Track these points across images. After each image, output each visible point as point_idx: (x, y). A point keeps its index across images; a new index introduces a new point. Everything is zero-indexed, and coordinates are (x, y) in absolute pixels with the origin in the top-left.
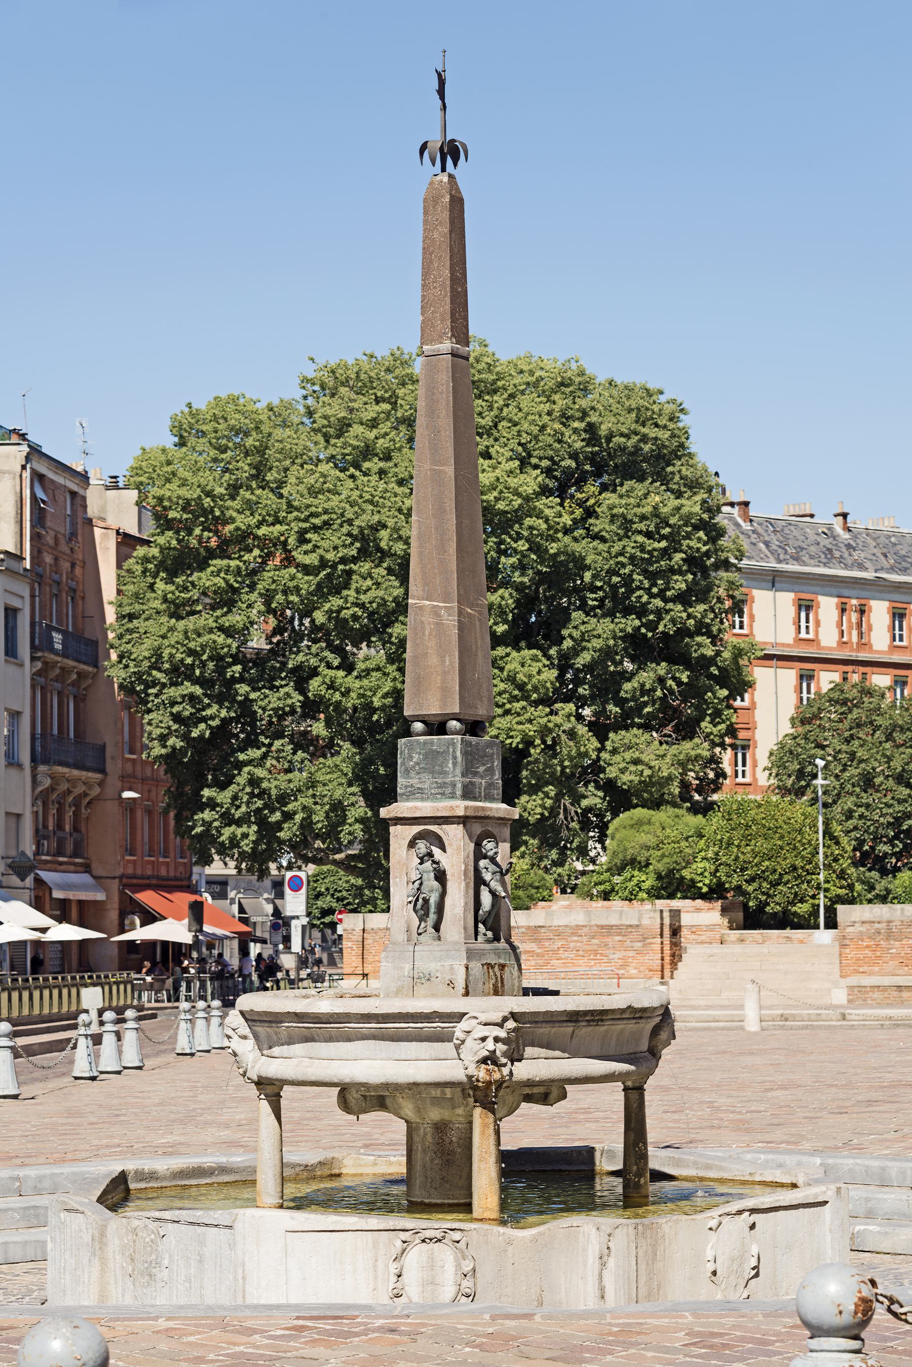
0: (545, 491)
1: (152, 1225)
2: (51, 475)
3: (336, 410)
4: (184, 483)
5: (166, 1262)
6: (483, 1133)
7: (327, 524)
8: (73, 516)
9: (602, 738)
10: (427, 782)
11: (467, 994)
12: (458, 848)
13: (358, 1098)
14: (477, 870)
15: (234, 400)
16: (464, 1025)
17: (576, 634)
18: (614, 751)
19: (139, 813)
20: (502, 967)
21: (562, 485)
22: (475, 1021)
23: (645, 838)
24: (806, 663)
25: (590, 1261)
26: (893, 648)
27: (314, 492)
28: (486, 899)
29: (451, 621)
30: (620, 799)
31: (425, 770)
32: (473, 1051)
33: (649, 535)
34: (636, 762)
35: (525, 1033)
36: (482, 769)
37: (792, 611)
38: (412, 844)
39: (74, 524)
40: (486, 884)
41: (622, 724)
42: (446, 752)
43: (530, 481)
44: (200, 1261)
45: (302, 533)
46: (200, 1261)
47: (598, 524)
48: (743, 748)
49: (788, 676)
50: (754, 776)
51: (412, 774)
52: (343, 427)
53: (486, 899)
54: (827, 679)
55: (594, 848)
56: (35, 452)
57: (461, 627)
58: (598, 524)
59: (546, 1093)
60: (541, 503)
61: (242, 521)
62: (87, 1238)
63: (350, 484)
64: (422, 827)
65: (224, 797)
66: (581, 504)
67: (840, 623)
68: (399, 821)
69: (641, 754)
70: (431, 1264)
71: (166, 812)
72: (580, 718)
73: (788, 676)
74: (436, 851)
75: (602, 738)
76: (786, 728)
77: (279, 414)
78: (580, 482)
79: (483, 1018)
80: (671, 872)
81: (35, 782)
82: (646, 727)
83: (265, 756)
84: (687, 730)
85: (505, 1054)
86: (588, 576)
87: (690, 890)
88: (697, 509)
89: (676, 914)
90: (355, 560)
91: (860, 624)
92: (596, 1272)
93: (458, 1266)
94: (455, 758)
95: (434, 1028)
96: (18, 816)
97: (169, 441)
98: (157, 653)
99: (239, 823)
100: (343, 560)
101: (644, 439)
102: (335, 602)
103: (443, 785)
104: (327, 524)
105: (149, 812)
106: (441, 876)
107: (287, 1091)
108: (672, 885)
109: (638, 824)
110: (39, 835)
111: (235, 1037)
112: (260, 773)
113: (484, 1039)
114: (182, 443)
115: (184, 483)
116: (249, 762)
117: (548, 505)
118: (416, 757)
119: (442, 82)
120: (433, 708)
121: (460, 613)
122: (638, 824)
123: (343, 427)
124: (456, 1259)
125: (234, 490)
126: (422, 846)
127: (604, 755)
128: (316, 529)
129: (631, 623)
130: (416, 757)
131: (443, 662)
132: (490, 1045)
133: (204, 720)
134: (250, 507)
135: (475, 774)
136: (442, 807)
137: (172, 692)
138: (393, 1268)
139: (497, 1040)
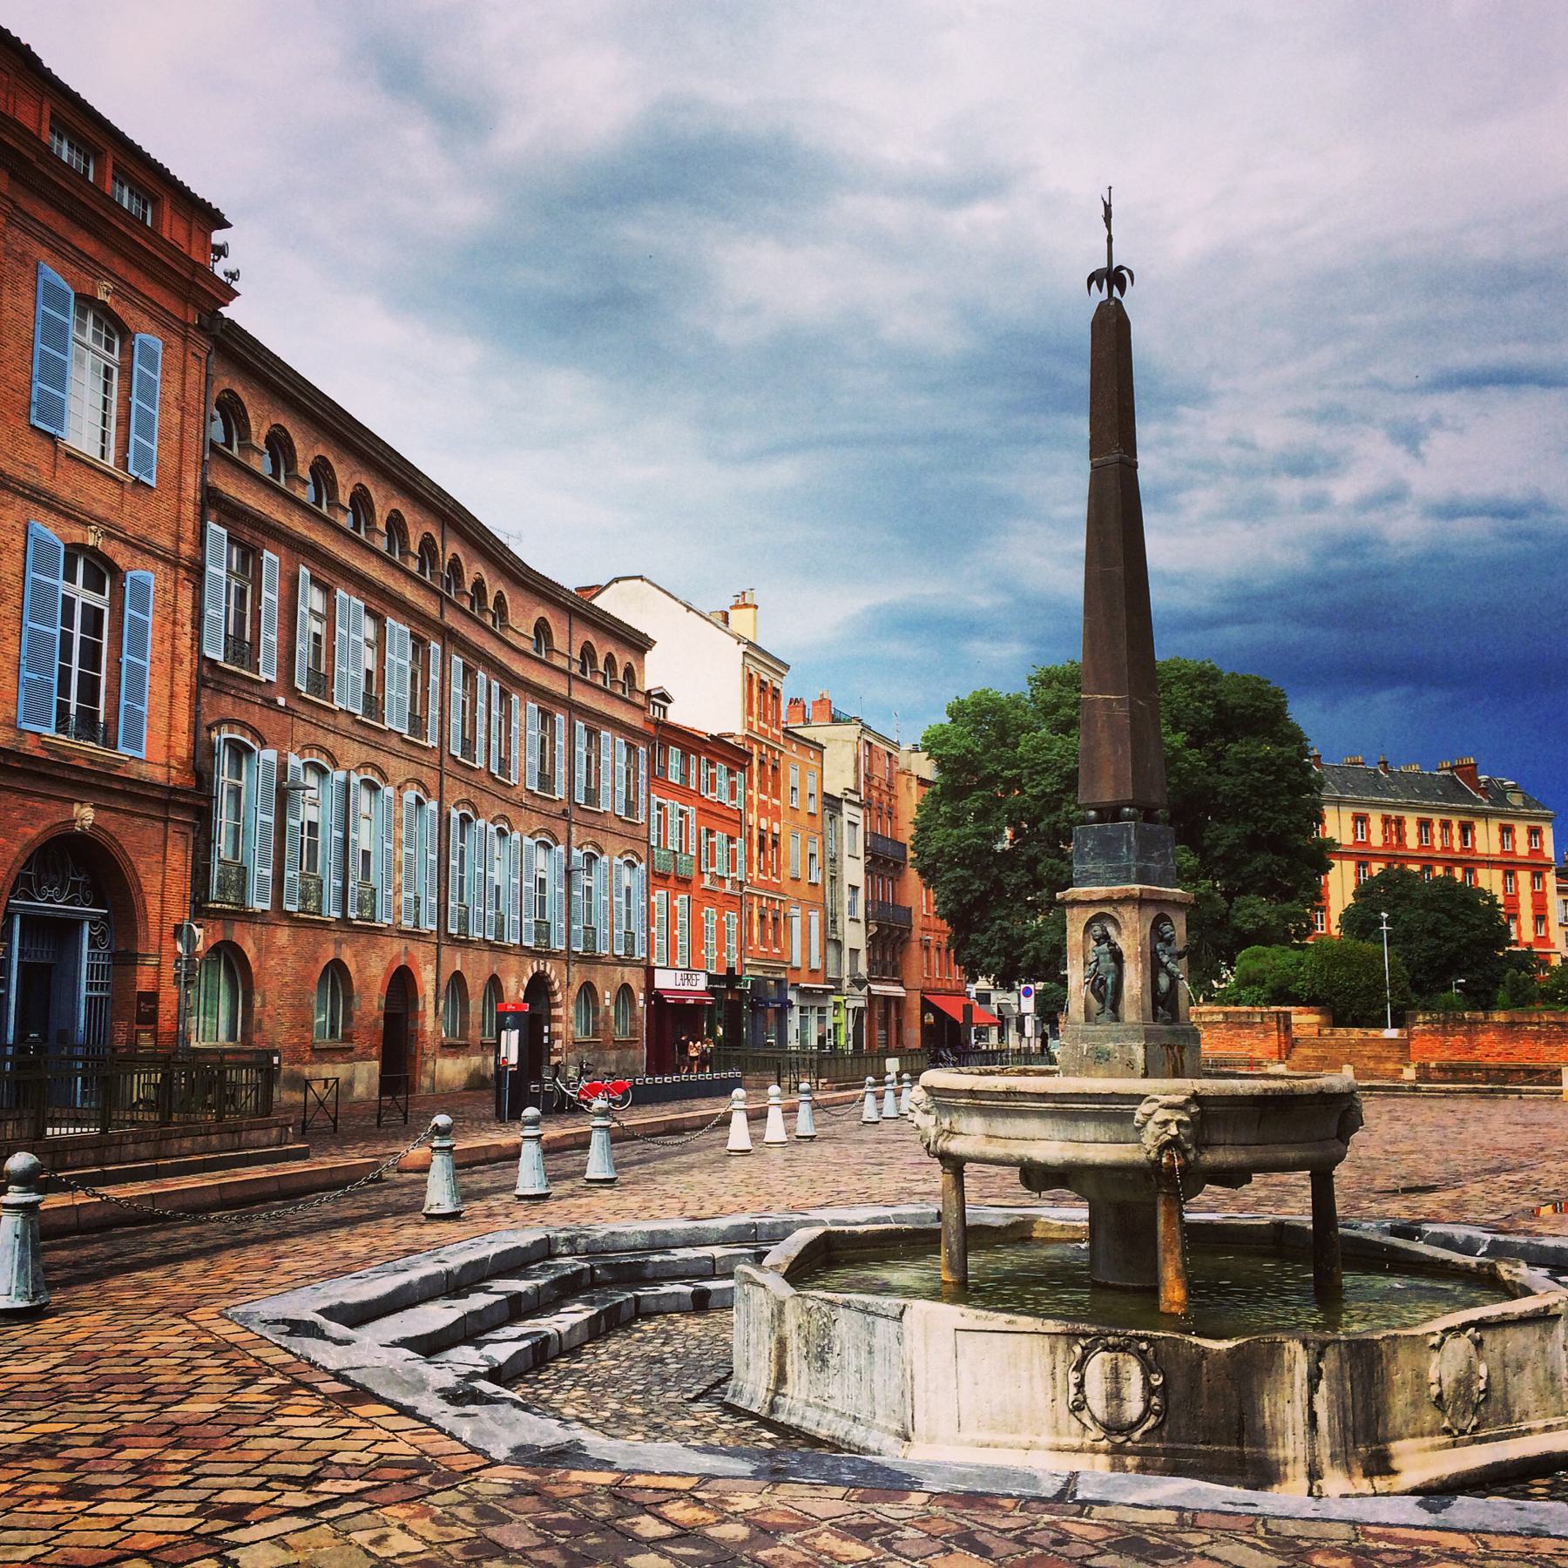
0: (1189, 745)
1: (825, 1308)
2: (875, 743)
3: (1048, 696)
4: (955, 746)
5: (837, 1349)
6: (1167, 1221)
7: (1046, 770)
8: (891, 768)
9: (1230, 901)
10: (1099, 866)
11: (1145, 1076)
12: (1134, 931)
13: (1038, 1177)
14: (1154, 952)
15: (985, 692)
16: (1145, 1108)
17: (1212, 835)
18: (1239, 909)
19: (933, 951)
20: (1181, 1049)
21: (1197, 740)
22: (1155, 1105)
23: (1259, 966)
24: (1363, 861)
25: (1298, 1383)
26: (1421, 848)
27: (1036, 750)
28: (1164, 981)
29: (1122, 712)
30: (1246, 940)
31: (1099, 855)
32: (1151, 1137)
33: (1261, 771)
34: (1253, 916)
35: (1208, 1117)
36: (1155, 854)
37: (1351, 824)
38: (1088, 926)
39: (891, 773)
40: (1164, 966)
41: (1243, 891)
42: (1120, 839)
43: (1179, 739)
44: (870, 1352)
45: (1030, 774)
46: (870, 1352)
47: (1225, 764)
48: (1324, 909)
49: (1350, 866)
50: (1331, 924)
51: (1088, 859)
52: (1056, 707)
53: (1164, 981)
54: (1376, 868)
55: (1226, 973)
56: (866, 729)
57: (1133, 717)
58: (1225, 764)
59: (1233, 1177)
60: (1187, 753)
61: (992, 768)
62: (767, 1314)
63: (1059, 744)
64: (1098, 910)
65: (983, 939)
66: (1213, 749)
67: (1384, 831)
68: (1076, 903)
69: (1258, 909)
70: (1116, 1375)
71: (948, 951)
72: (1214, 888)
73: (1350, 866)
74: (1111, 930)
75: (1230, 901)
76: (1350, 900)
77: (1015, 703)
78: (1211, 738)
79: (1165, 1100)
80: (1281, 988)
81: (867, 930)
82: (1261, 894)
83: (1009, 915)
84: (1288, 895)
85: (1188, 1140)
86: (1220, 799)
87: (1295, 1000)
88: (1294, 754)
89: (1287, 1015)
90: (1063, 791)
91: (1398, 830)
92: (1306, 1396)
93: (1146, 1381)
94: (1129, 842)
95: (1113, 1111)
96: (858, 951)
97: (947, 720)
98: (941, 850)
99: (992, 955)
100: (1057, 791)
101: (1258, 709)
102: (1053, 818)
103: (1118, 870)
104: (1046, 770)
105: (939, 949)
106: (1117, 957)
107: (968, 1167)
108: (1282, 996)
109: (1257, 956)
110: (870, 963)
111: (919, 1112)
112: (1006, 924)
113: (1165, 1123)
114: (954, 721)
115: (955, 746)
116: (1000, 918)
117: (1193, 755)
118: (1090, 844)
119: (1108, 208)
120: (1107, 797)
121: (1131, 704)
122: (1257, 956)
123: (1056, 707)
124: (1143, 1371)
125: (986, 749)
126: (1097, 929)
127: (1232, 912)
128: (1037, 773)
129: (1249, 828)
130: (1090, 844)
131: (1116, 752)
132: (1173, 1130)
133: (971, 892)
134: (998, 759)
135: (1150, 859)
136: (1118, 889)
137: (949, 875)
138: (1074, 1377)
139: (1179, 1123)
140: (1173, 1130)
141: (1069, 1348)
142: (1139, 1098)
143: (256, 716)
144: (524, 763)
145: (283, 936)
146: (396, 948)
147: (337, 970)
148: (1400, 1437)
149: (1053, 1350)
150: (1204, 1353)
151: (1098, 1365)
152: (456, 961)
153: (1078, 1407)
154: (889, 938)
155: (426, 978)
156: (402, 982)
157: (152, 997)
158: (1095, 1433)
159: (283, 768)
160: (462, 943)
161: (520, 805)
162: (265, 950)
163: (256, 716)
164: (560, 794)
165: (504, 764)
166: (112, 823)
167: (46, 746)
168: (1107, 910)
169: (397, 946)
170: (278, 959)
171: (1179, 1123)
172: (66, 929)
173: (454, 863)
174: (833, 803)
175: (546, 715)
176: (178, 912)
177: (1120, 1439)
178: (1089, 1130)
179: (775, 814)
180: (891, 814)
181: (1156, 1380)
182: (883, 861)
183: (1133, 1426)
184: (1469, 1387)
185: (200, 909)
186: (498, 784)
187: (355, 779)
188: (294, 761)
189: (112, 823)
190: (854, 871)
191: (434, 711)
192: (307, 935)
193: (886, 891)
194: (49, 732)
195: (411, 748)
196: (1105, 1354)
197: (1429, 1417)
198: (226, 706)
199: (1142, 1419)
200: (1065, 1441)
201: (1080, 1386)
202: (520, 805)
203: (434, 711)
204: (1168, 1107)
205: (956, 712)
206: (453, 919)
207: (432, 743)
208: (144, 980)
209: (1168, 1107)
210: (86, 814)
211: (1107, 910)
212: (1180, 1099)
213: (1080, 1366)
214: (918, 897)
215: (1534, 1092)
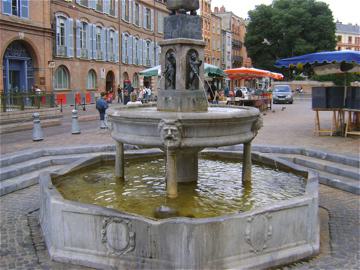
16: (160, 124)
70: (117, 231)
79: (168, 121)
93: (128, 234)
95: (150, 124)
113: (167, 130)
140: (169, 133)
141: (101, 220)
142: (159, 120)
143: (67, 10)
144: (143, 24)
145: (78, 64)
146: (109, 67)
147: (92, 72)
148: (230, 256)
149: (95, 221)
150: (149, 226)
151: (111, 227)
152: (125, 69)
153: (104, 242)
154: (237, 63)
155: (117, 74)
156: (110, 75)
157: (44, 78)
158: (111, 251)
159: (75, 23)
160: (127, 65)
161: (141, 32)
162: (72, 67)
163: (67, 10)
164: (152, 29)
165: (137, 23)
166: (28, 36)
167: (10, 18)
168: (171, 47)
169: (109, 66)
170: (76, 69)
171: (172, 130)
172: (21, 62)
173: (124, 46)
174: (224, 32)
175: (148, 10)
176: (49, 58)
177: (119, 254)
178: (144, 131)
179: (209, 35)
180: (239, 35)
181: (132, 235)
182: (236, 46)
183: (124, 250)
184: (263, 235)
185: (54, 57)
186: (136, 27)
187: (95, 26)
188: (78, 21)
189: (28, 36)
190: (229, 48)
191: (116, 9)
192: (84, 63)
193: (237, 53)
194: (11, 15)
195: (111, 18)
196: (115, 224)
197: (247, 247)
198: (59, 8)
199: (127, 247)
200: (99, 253)
201: (105, 234)
202: (141, 32)
203: (116, 9)
204: (168, 124)
205: (258, 8)
206: (124, 59)
207: (116, 17)
208: (41, 74)
209: (168, 124)
210: (22, 35)
211: (171, 47)
212: (172, 121)
213: (105, 227)
214: (244, 53)
215: (216, 146)
